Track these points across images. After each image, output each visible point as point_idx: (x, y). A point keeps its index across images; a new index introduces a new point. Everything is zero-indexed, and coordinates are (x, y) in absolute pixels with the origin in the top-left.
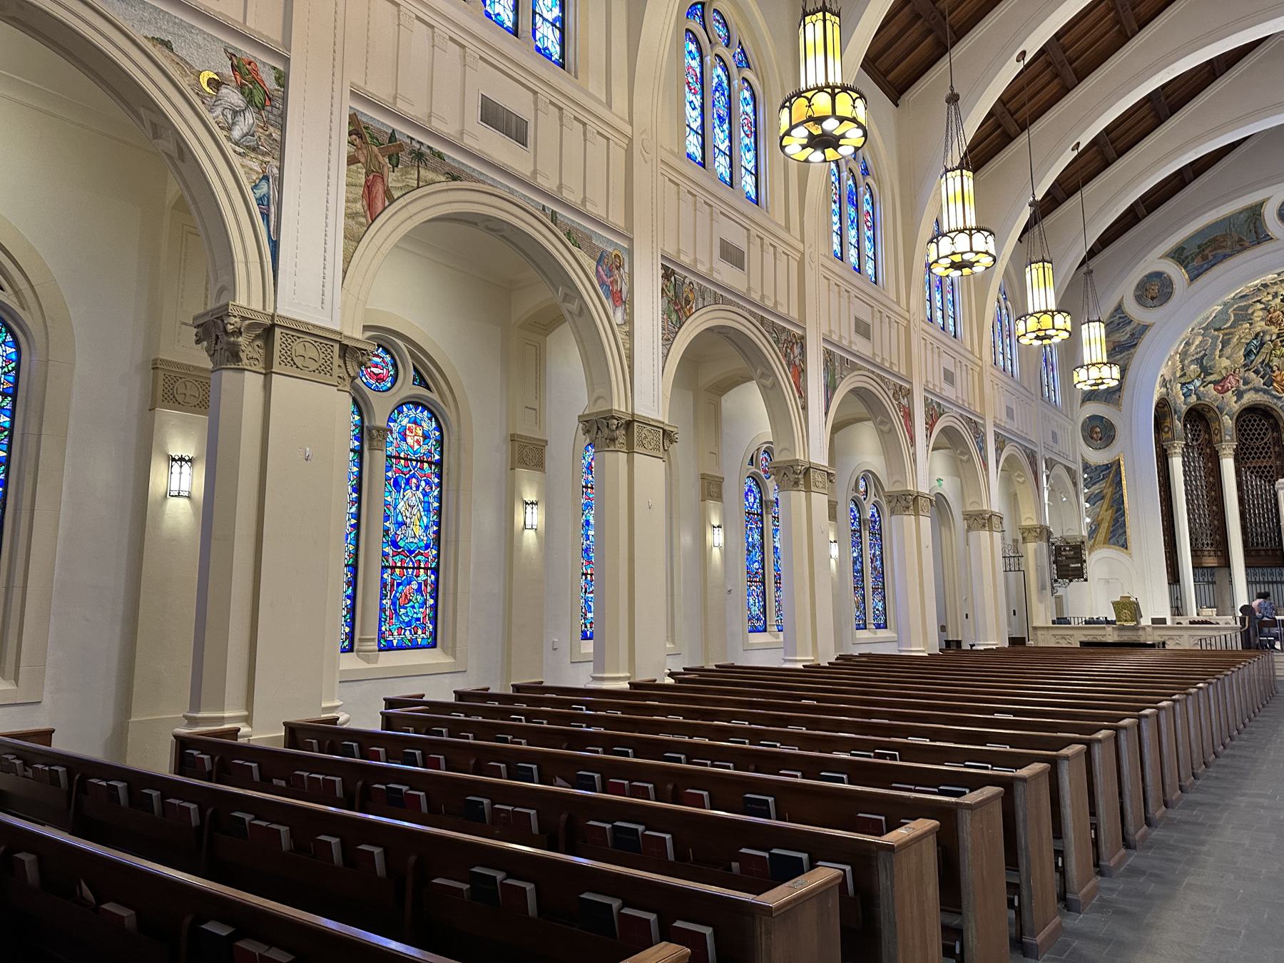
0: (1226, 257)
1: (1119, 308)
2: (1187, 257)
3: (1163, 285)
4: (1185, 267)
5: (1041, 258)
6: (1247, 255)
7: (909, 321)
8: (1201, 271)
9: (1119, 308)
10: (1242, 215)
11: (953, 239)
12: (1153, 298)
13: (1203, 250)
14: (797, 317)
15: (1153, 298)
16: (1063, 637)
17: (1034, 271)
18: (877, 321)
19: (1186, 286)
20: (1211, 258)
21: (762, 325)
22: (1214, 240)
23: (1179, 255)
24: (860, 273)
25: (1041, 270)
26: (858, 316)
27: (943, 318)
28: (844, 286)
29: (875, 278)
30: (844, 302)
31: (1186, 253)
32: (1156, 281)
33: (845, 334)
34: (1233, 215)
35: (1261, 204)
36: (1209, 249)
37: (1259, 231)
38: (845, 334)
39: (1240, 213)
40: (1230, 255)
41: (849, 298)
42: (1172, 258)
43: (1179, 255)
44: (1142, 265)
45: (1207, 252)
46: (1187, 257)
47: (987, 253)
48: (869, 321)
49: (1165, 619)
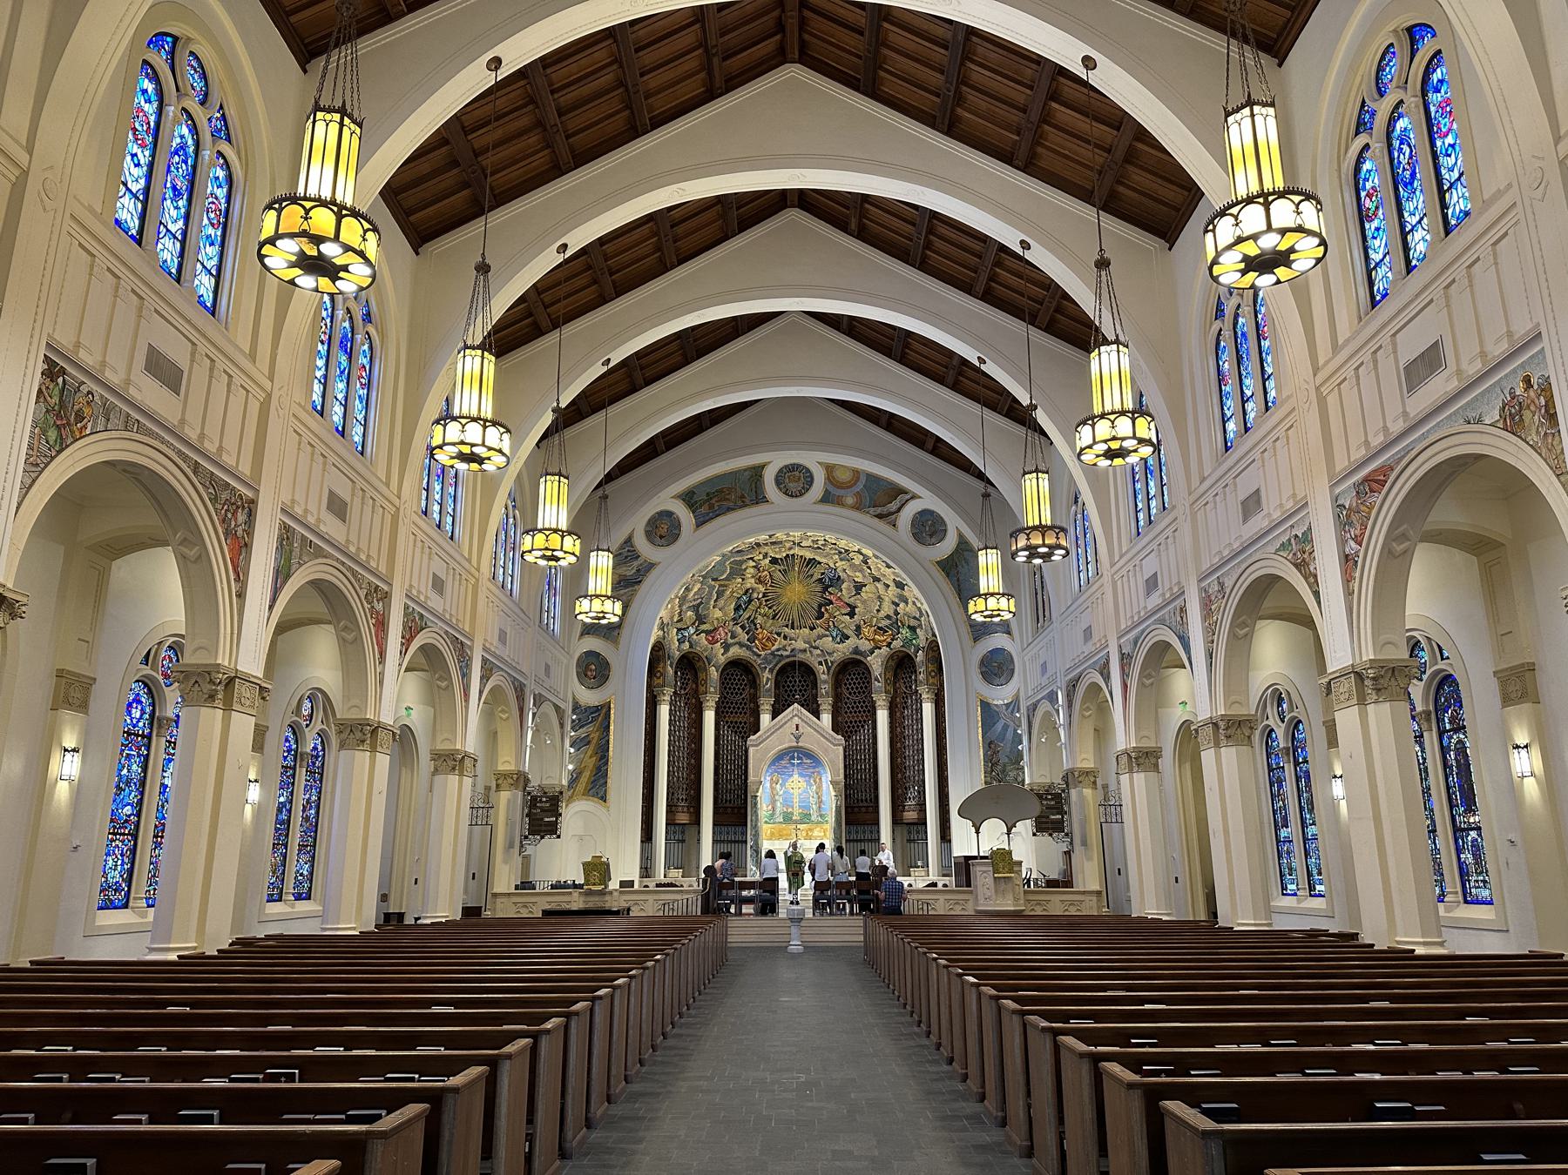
0: (729, 510)
2: (696, 502)
4: (693, 512)
10: (747, 473)
12: (661, 537)
15: (661, 537)
18: (357, 501)
20: (716, 508)
22: (721, 491)
23: (688, 498)
25: (556, 483)
26: (334, 489)
28: (320, 447)
29: (363, 447)
30: (317, 467)
31: (696, 498)
37: (759, 492)
38: (312, 507)
39: (745, 470)
40: (733, 509)
42: (684, 500)
43: (688, 498)
44: (655, 500)
45: (713, 501)
46: (696, 502)
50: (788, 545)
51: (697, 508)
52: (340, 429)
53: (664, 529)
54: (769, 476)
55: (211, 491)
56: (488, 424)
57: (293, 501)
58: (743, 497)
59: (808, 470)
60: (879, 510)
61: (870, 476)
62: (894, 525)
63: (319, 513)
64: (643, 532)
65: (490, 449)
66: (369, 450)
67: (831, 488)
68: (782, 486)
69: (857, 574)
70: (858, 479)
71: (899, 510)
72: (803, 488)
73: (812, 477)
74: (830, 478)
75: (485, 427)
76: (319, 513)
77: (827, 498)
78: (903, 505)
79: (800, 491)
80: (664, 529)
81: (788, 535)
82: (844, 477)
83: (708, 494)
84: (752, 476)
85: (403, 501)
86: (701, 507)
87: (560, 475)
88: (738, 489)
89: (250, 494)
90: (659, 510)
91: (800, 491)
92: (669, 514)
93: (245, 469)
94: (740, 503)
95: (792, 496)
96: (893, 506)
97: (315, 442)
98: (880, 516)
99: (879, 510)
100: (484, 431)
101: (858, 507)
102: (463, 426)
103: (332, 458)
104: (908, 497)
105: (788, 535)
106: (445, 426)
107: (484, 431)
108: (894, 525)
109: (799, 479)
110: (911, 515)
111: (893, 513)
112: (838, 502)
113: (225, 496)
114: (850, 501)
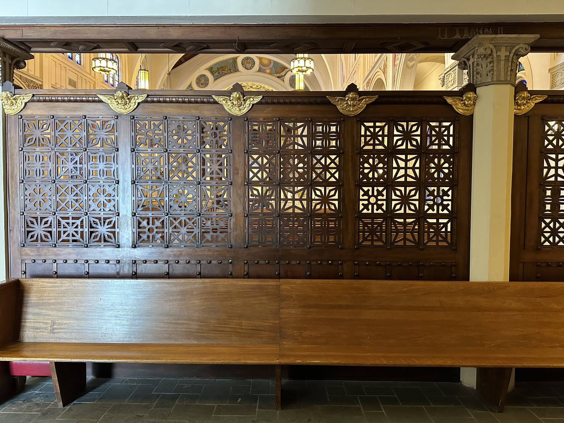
0: (226, 74)
1: (190, 85)
2: (213, 71)
3: (206, 80)
4: (213, 75)
5: (144, 69)
6: (232, 75)
7: (95, 82)
8: (218, 77)
9: (190, 85)
10: (231, 60)
11: (100, 61)
12: (202, 84)
13: (219, 70)
14: (39, 76)
15: (202, 84)
16: (423, 170)
17: (142, 73)
18: (80, 81)
19: (213, 82)
20: (221, 73)
21: (20, 79)
22: (222, 67)
23: (211, 69)
24: (72, 60)
25: (144, 73)
26: (70, 78)
27: (113, 81)
28: (63, 65)
29: (80, 62)
30: (63, 72)
31: (213, 70)
32: (203, 78)
33: (63, 84)
34: (227, 60)
35: (237, 58)
36: (221, 70)
37: (236, 67)
38: (63, 84)
39: (230, 59)
40: (227, 74)
41: (66, 70)
42: (209, 70)
43: (211, 69)
44: (198, 71)
45: (220, 71)
46: (213, 71)
47: (113, 69)
48: (76, 80)
49: (72, 219)
50: (248, 87)
51: (214, 74)
52: (71, 57)
53: (203, 81)
54: (239, 61)
55: (27, 83)
56: (108, 60)
57: (56, 83)
58: (230, 69)
59: (253, 60)
60: (278, 75)
61: (274, 62)
62: (283, 81)
63: (66, 86)
64: (195, 83)
65: (109, 68)
66: (82, 63)
67: (261, 66)
68: (244, 65)
69: (496, 63)
70: (271, 63)
71: (285, 75)
72: (251, 66)
73: (254, 62)
74: (261, 63)
75: (107, 61)
76: (66, 86)
77: (260, 70)
78: (286, 73)
79: (250, 67)
80: (203, 81)
81: (247, 84)
82: (265, 62)
83: (218, 68)
84: (233, 62)
85: (96, 79)
86: (215, 73)
87: (145, 70)
88: (228, 66)
89: (40, 83)
90: (200, 74)
91: (250, 67)
92: (204, 76)
93: (38, 75)
94: (229, 72)
95: (247, 69)
96: (283, 74)
97: (61, 63)
98: (278, 77)
99: (278, 75)
100: (107, 62)
101: (271, 74)
102: (100, 61)
103: (68, 68)
104: (288, 70)
105: (247, 84)
106: (95, 61)
107: (107, 62)
108: (283, 81)
109: (250, 62)
110: (289, 77)
111: (283, 76)
112: (264, 72)
113: (32, 84)
114: (268, 71)
